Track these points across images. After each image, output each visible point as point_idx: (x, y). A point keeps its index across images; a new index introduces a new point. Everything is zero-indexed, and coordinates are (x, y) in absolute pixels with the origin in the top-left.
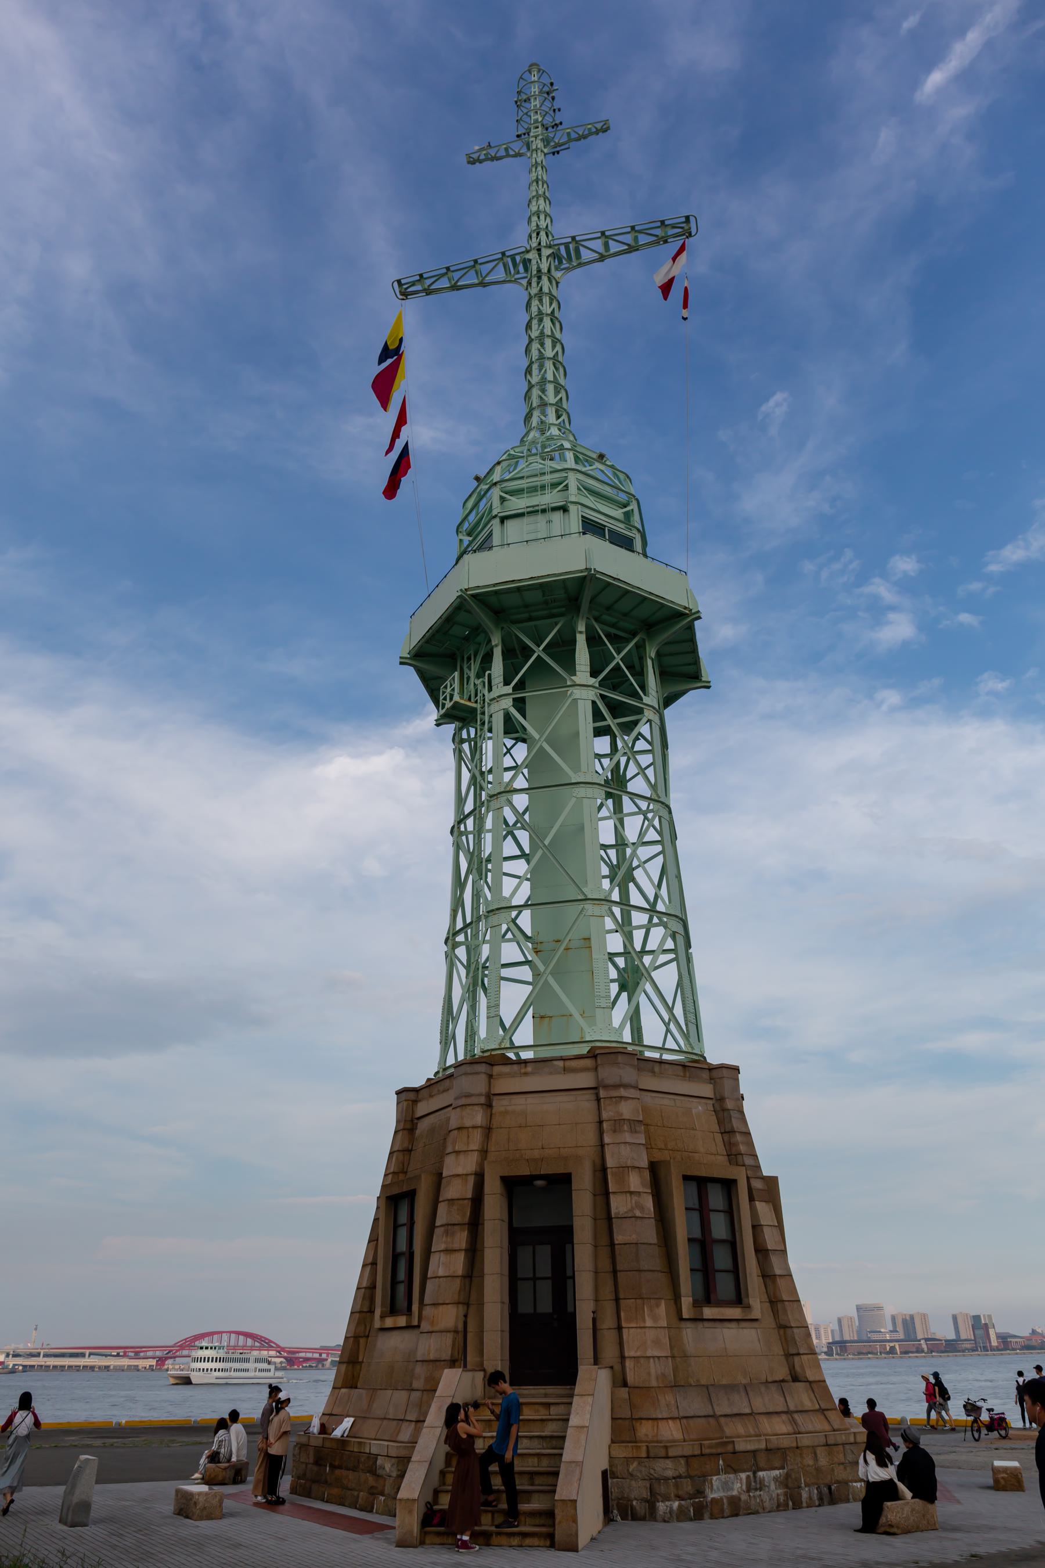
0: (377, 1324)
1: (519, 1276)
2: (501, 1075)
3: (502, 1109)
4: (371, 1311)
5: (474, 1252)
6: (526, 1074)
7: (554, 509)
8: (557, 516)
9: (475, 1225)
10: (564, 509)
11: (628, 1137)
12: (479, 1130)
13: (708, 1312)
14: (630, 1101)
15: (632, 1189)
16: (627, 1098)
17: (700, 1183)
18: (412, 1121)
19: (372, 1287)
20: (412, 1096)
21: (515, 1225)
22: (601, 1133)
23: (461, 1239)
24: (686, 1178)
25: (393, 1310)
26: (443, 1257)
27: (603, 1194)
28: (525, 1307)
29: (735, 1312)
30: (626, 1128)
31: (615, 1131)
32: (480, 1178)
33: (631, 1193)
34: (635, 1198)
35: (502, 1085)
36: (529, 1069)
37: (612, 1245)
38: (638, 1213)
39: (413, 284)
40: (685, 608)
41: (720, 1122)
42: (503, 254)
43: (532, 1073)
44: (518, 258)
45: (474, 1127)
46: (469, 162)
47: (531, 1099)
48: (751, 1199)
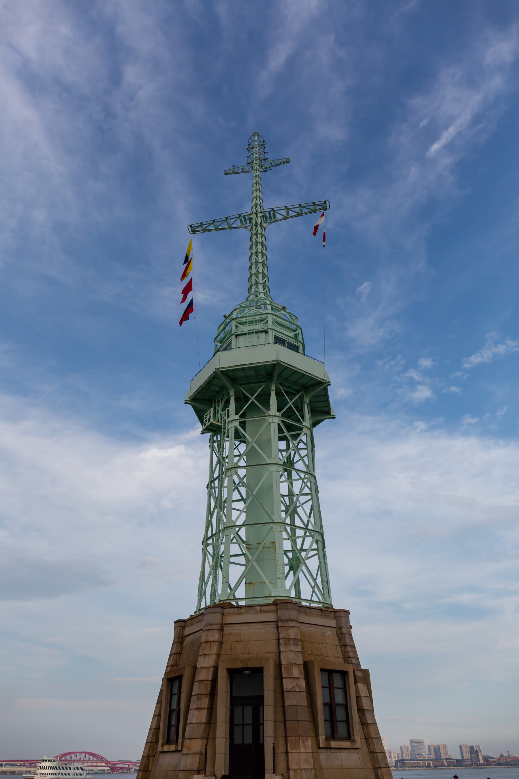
0: (160, 749)
1: (235, 723)
2: (229, 614)
3: (228, 632)
4: (157, 742)
5: (212, 709)
6: (241, 613)
7: (261, 332)
8: (263, 335)
9: (213, 694)
10: (266, 332)
11: (293, 648)
12: (216, 643)
13: (333, 744)
14: (294, 628)
15: (295, 676)
16: (292, 627)
17: (330, 673)
18: (182, 638)
19: (158, 728)
20: (182, 624)
21: (234, 695)
22: (279, 645)
23: (205, 702)
24: (322, 670)
25: (168, 742)
26: (196, 713)
27: (279, 678)
28: (238, 741)
29: (346, 744)
30: (292, 643)
31: (286, 645)
32: (216, 668)
33: (294, 678)
34: (296, 681)
35: (229, 619)
36: (243, 611)
37: (284, 706)
38: (297, 689)
39: (198, 227)
40: (323, 380)
41: (340, 640)
42: (240, 215)
43: (245, 613)
44: (247, 217)
45: (214, 642)
46: (225, 174)
47: (243, 627)
48: (356, 682)
